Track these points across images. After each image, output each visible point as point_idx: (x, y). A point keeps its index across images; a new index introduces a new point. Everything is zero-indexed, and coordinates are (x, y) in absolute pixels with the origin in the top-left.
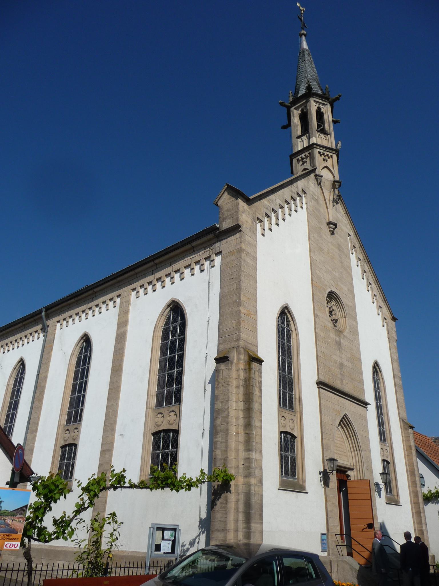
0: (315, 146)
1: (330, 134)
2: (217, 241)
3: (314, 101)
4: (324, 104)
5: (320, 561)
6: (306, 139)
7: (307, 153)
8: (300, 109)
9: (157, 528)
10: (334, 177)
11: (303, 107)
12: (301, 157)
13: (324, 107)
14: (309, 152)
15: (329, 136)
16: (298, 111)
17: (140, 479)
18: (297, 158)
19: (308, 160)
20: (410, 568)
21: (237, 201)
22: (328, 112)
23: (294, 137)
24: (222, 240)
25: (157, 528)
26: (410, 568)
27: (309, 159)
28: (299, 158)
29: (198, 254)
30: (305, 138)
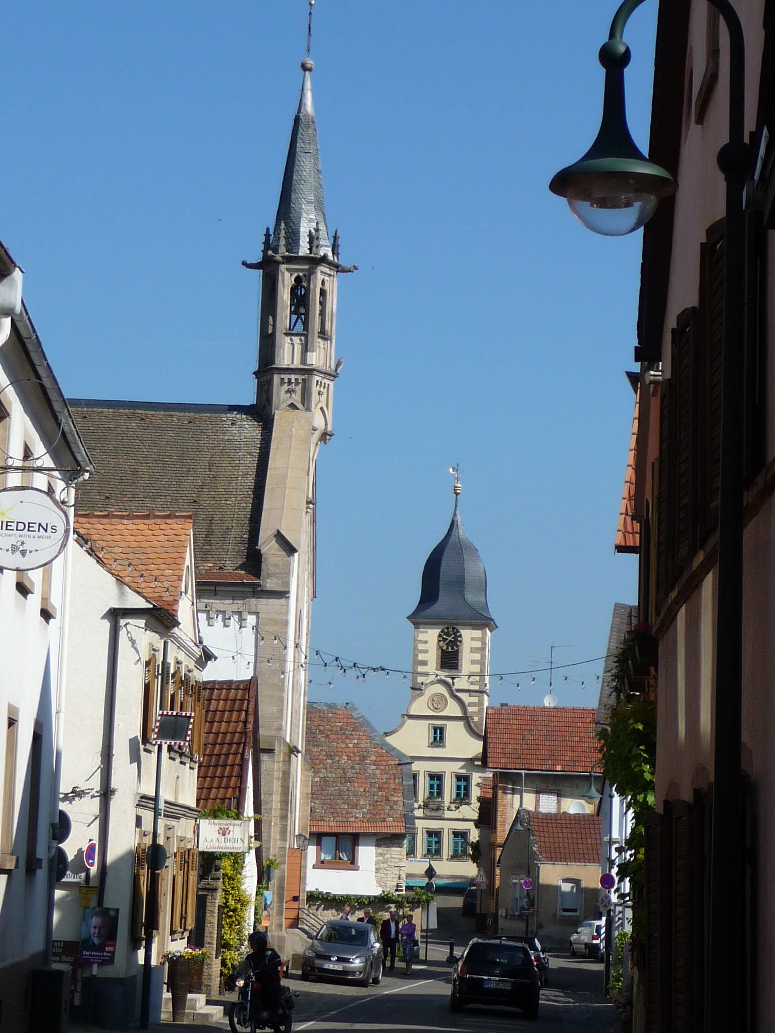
0: (315, 372)
1: (331, 340)
2: (253, 597)
3: (322, 272)
4: (330, 275)
5: (70, 942)
6: (298, 344)
7: (300, 378)
8: (296, 275)
9: (118, 909)
10: (326, 424)
11: (301, 274)
12: (290, 380)
13: (328, 279)
14: (303, 377)
15: (329, 342)
16: (291, 275)
17: (50, 821)
18: (282, 376)
19: (299, 389)
20: (281, 1027)
21: (288, 559)
22: (333, 293)
23: (280, 330)
24: (261, 598)
25: (118, 909)
26: (281, 1027)
27: (300, 388)
28: (286, 377)
29: (223, 601)
30: (298, 342)
